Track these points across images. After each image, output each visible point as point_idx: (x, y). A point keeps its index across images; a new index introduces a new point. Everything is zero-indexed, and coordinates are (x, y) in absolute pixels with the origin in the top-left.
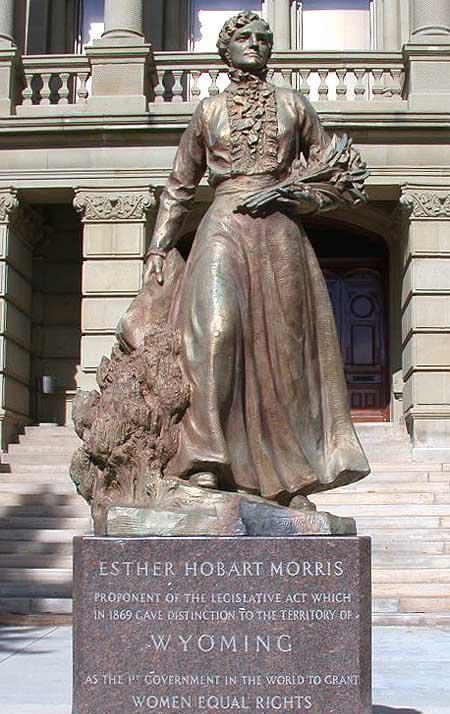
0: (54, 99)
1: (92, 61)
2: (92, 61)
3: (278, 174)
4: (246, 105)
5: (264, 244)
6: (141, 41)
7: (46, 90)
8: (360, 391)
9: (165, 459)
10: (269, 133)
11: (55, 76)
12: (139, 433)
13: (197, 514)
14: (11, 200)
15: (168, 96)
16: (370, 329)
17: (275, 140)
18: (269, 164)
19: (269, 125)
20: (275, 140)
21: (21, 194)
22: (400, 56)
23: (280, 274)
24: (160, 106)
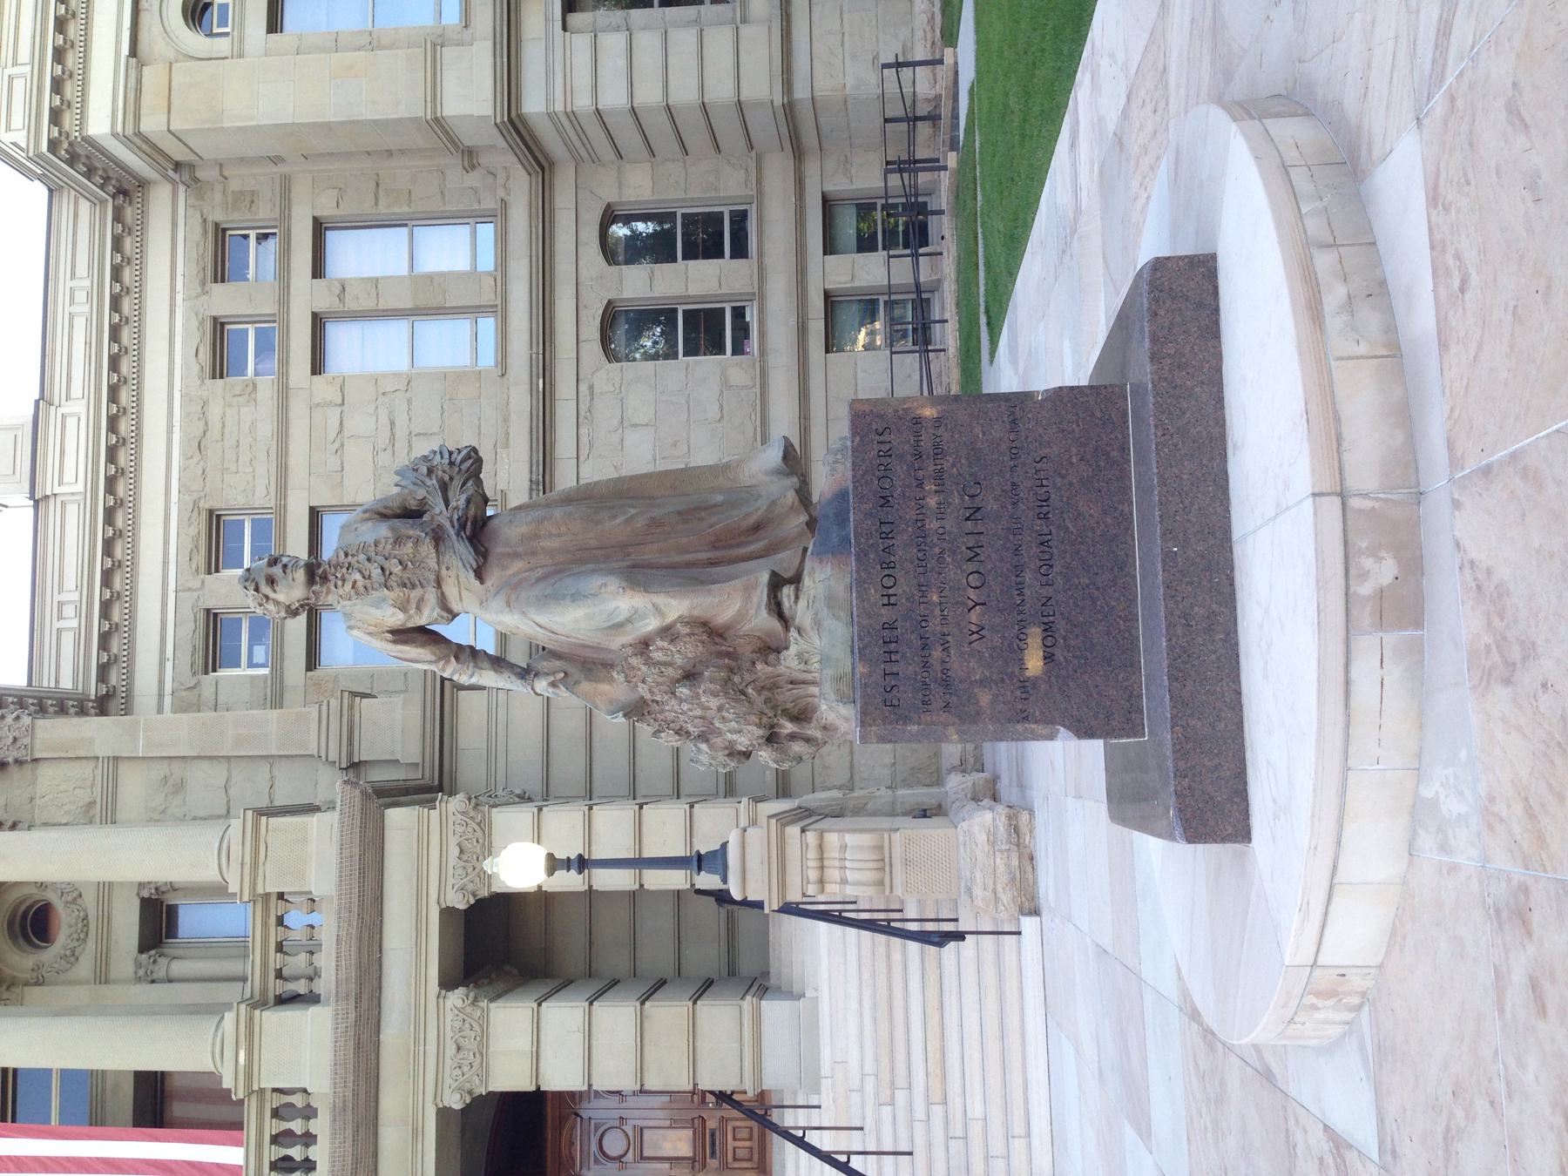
0: (309, 1139)
1: (256, 1087)
2: (256, 1087)
3: (438, 538)
4: (358, 576)
5: (520, 550)
6: (229, 1017)
7: (297, 1126)
8: (730, 1148)
9: (770, 649)
10: (389, 547)
11: (275, 1140)
12: (737, 679)
13: (830, 600)
14: (456, 997)
15: (309, 1139)
16: (646, 1154)
17: (398, 541)
18: (427, 548)
19: (381, 547)
20: (398, 541)
21: (447, 984)
22: (259, 905)
23: (555, 531)
24: (324, 986)
